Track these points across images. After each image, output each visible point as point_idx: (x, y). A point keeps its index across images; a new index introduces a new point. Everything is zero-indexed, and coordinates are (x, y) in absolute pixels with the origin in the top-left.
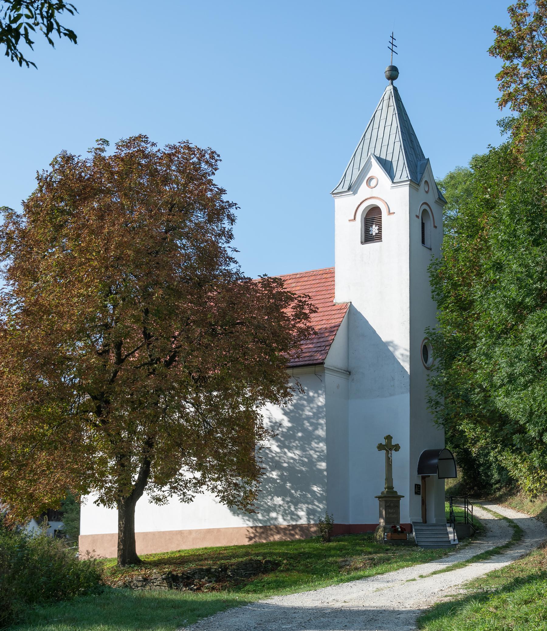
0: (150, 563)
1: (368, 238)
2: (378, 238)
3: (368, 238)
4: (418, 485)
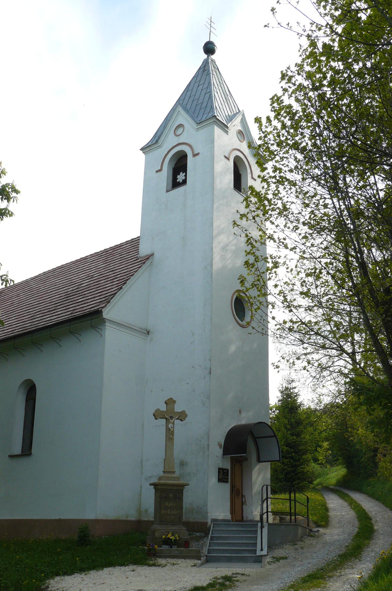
3: (175, 184)
4: (223, 469)
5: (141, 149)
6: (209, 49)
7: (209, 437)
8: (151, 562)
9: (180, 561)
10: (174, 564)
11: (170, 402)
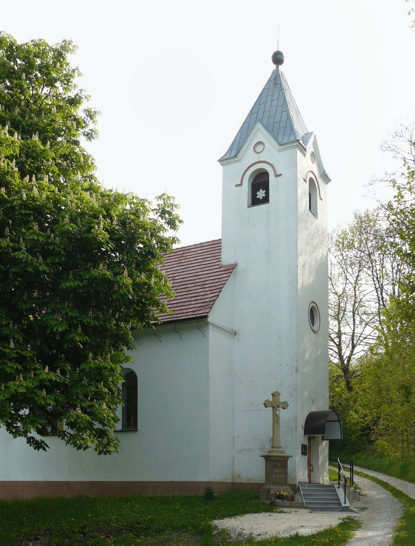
0: (306, 508)
1: (255, 201)
2: (266, 200)
3: (255, 201)
4: (305, 445)
5: (220, 161)
6: (278, 59)
7: (296, 422)
8: (278, 511)
9: (299, 510)
10: (296, 512)
11: (275, 395)
